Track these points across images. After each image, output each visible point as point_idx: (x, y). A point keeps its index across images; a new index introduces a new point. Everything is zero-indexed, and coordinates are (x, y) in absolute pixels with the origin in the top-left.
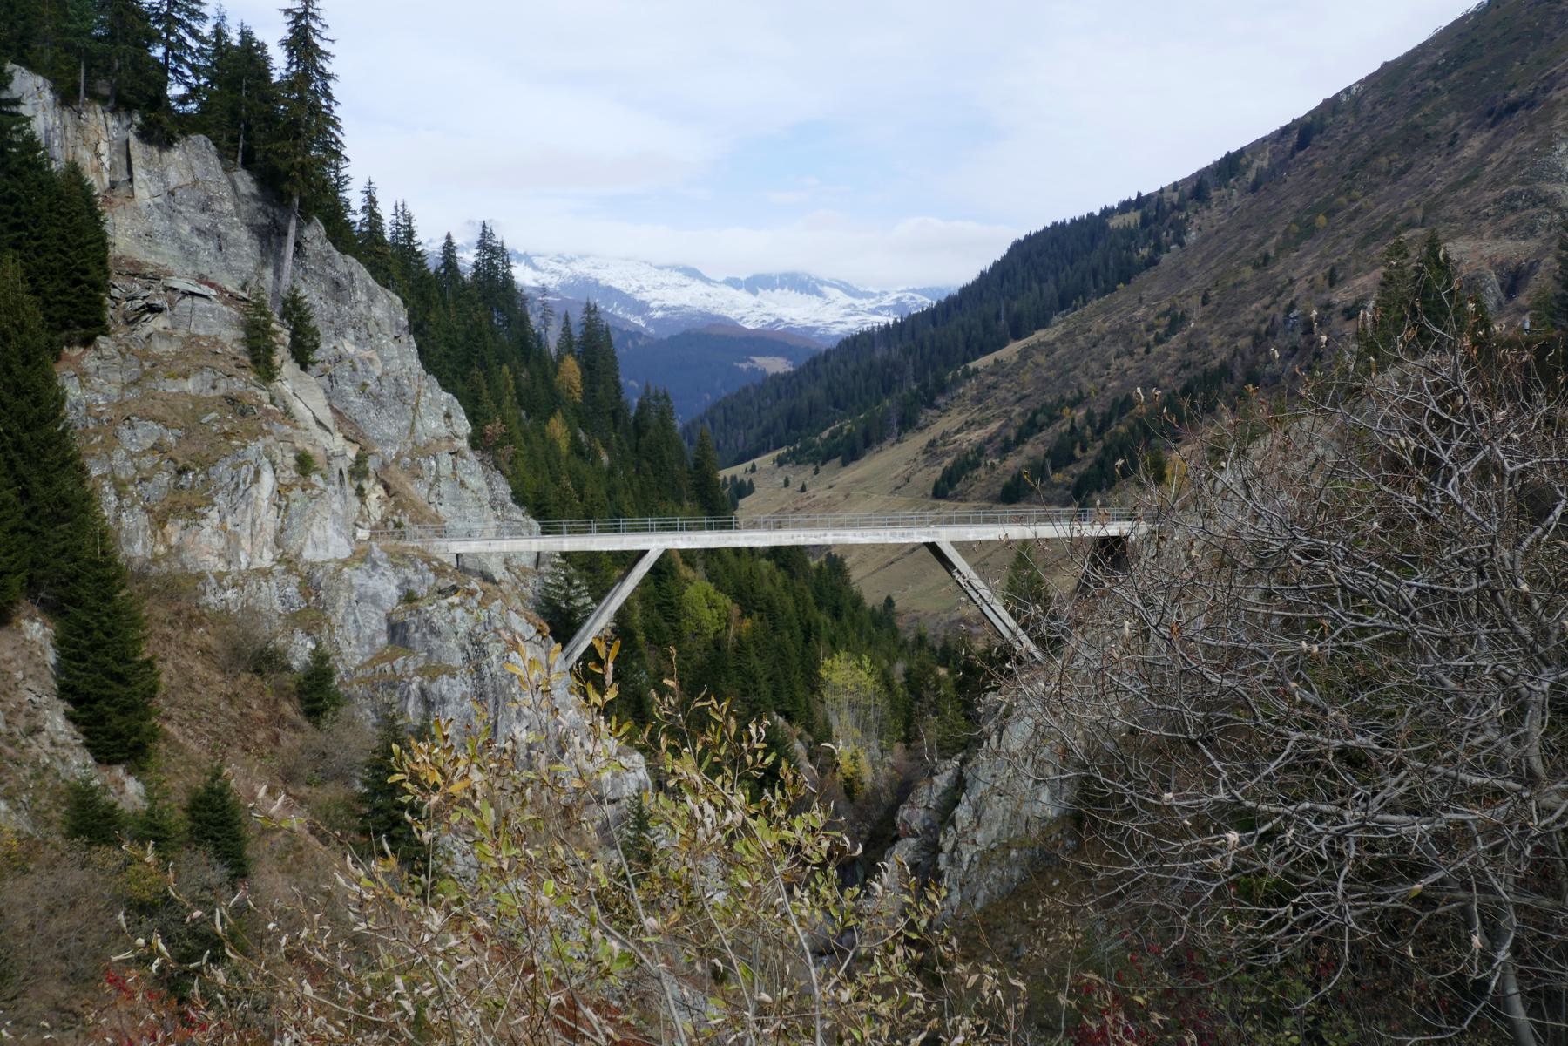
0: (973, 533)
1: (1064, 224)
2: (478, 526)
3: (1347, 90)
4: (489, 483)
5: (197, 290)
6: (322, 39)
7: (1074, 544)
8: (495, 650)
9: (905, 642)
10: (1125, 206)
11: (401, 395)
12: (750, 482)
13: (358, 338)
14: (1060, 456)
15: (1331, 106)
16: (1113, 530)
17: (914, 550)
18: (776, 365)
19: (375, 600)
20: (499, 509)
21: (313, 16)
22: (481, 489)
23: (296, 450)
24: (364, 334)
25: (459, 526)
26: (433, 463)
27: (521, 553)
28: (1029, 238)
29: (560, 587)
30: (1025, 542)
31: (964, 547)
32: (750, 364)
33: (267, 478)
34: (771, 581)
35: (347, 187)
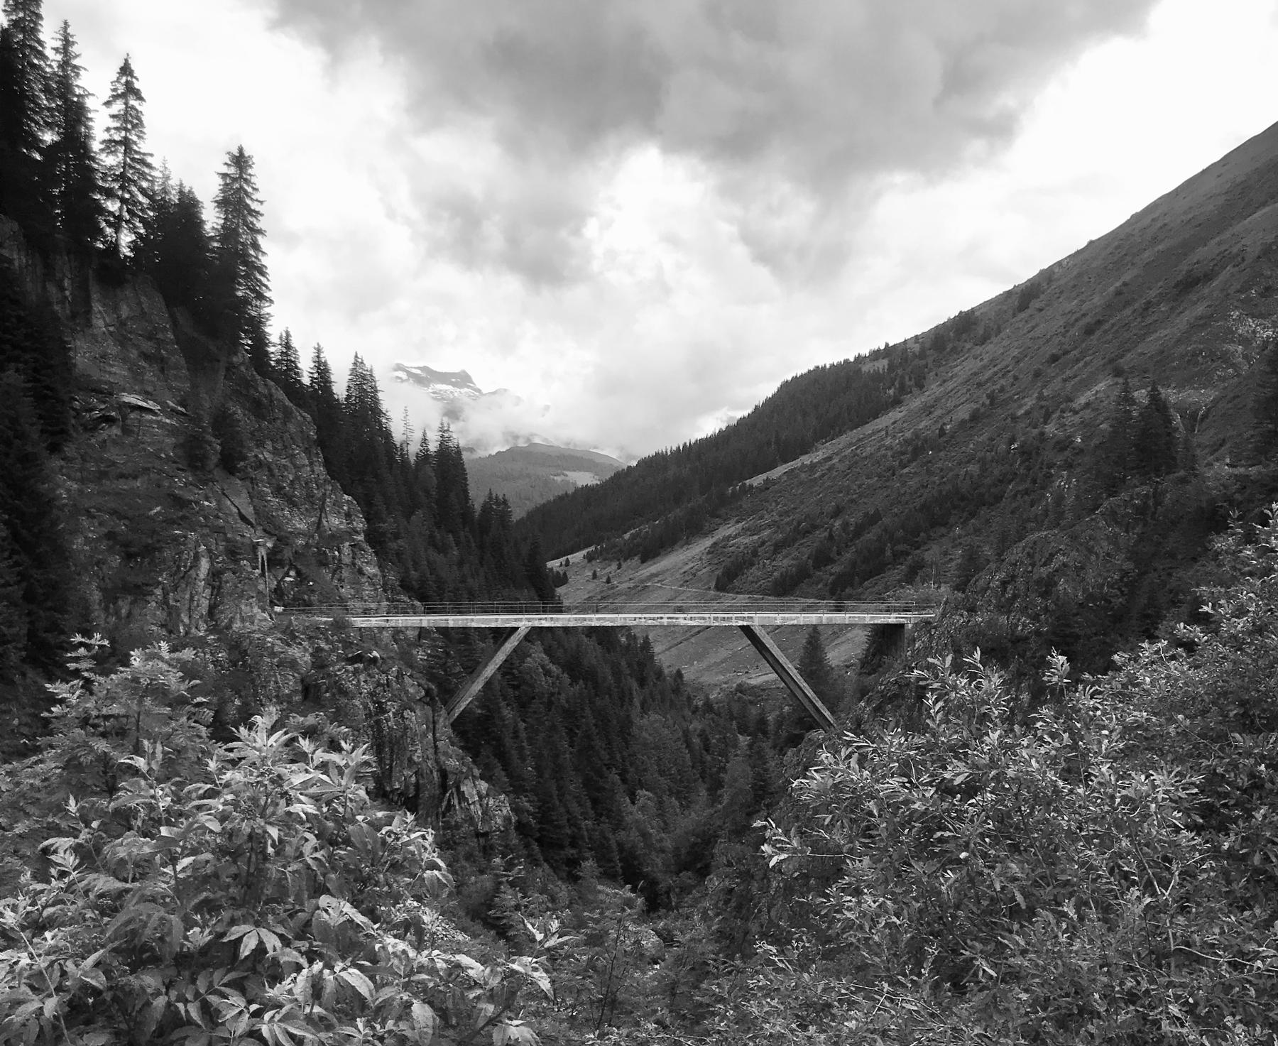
0: (779, 618)
1: (824, 368)
2: (373, 606)
3: (1059, 263)
4: (382, 571)
5: (144, 404)
6: (252, 199)
7: (423, 632)
8: (392, 707)
9: (697, 708)
10: (876, 355)
11: (310, 496)
12: (565, 574)
13: (275, 448)
14: (822, 559)
15: (1047, 276)
16: (892, 619)
17: (699, 632)
18: (585, 479)
19: (293, 664)
20: (389, 592)
21: (246, 180)
22: (375, 575)
23: (227, 540)
24: (279, 446)
25: (358, 604)
26: (336, 553)
27: (407, 628)
28: (795, 379)
29: (440, 658)
30: (815, 627)
31: (775, 630)
32: (563, 477)
33: (205, 564)
34: (592, 653)
35: (268, 323)
